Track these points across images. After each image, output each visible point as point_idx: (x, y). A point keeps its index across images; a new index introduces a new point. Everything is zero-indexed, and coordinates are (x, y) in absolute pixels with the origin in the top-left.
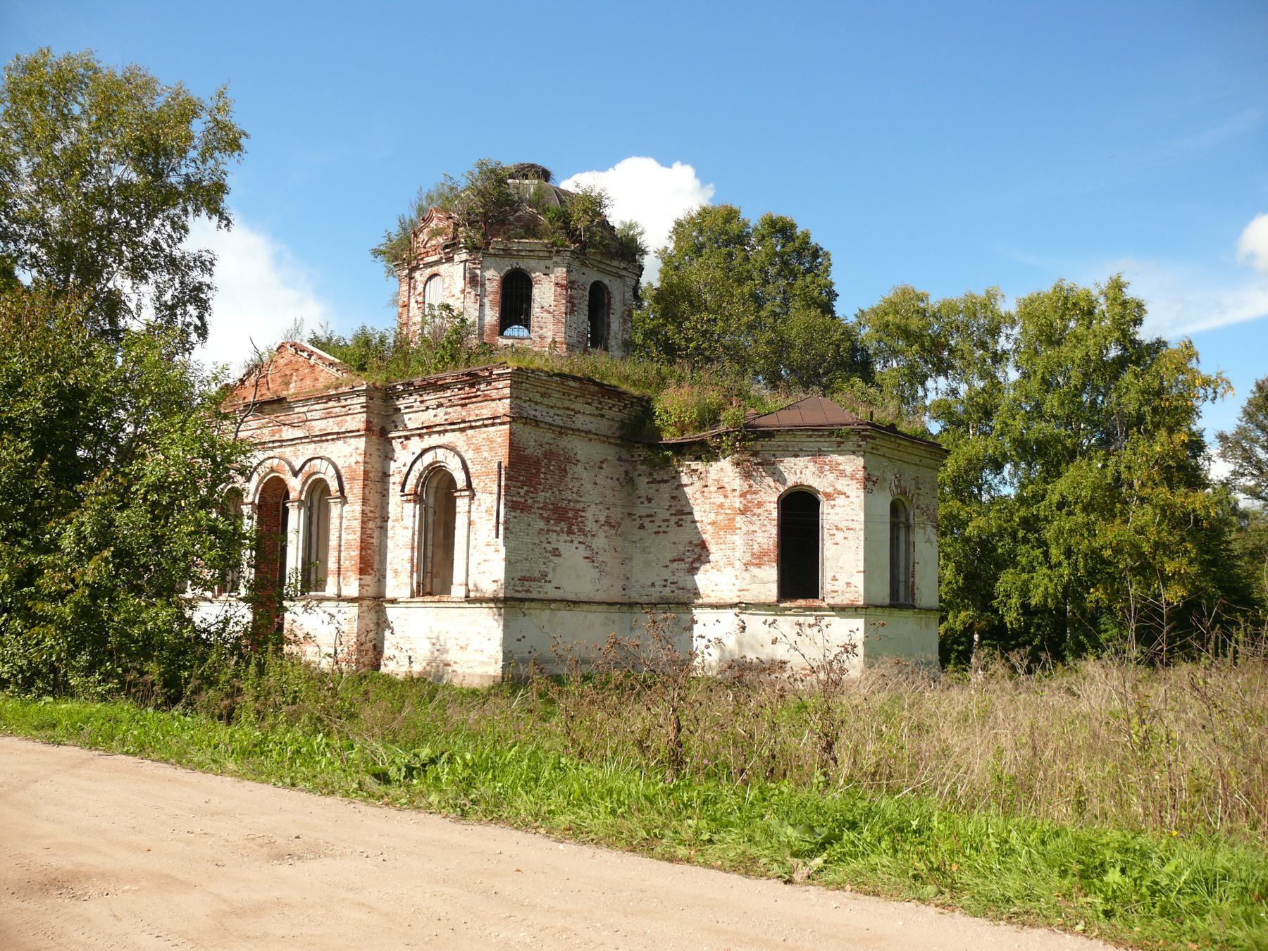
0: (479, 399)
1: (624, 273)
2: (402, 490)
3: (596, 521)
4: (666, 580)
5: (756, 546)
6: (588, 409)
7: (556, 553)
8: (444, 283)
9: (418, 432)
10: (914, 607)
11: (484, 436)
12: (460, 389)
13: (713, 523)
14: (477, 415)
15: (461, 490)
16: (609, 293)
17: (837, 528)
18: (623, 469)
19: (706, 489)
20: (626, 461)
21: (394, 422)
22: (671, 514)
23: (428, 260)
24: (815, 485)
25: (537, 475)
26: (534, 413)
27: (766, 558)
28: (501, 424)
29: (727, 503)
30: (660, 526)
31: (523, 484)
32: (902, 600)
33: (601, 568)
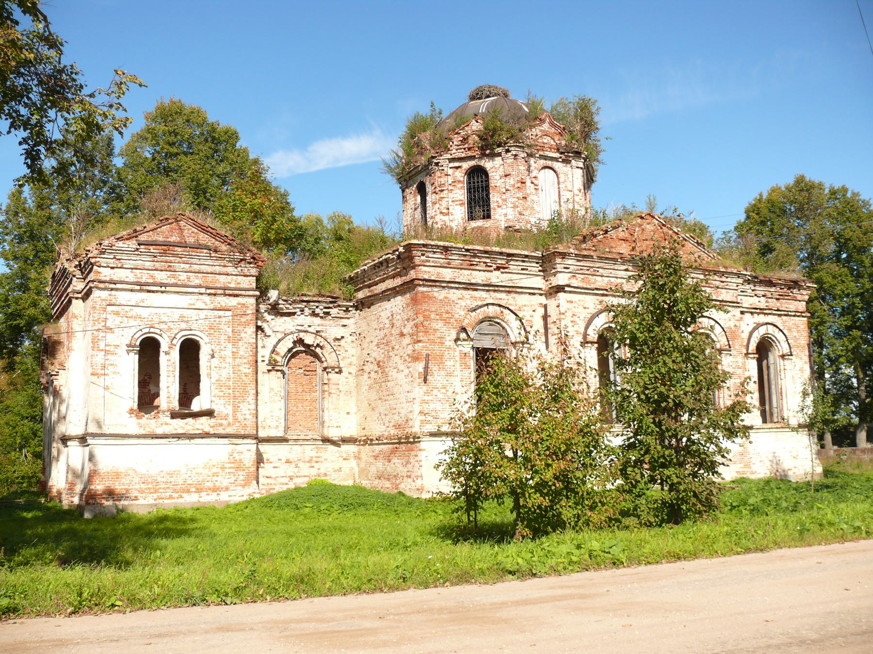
0: (789, 298)
11: (793, 322)
12: (781, 289)
28: (803, 317)
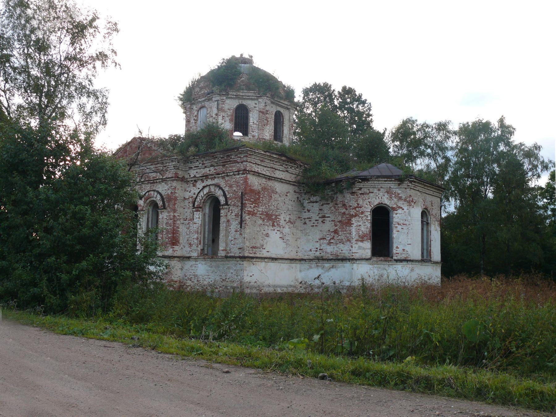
1: (289, 107)
2: (194, 205)
3: (285, 221)
4: (317, 248)
5: (361, 232)
6: (281, 168)
7: (267, 235)
8: (207, 110)
9: (201, 178)
10: (431, 261)
13: (340, 222)
14: (231, 170)
15: (223, 205)
16: (283, 116)
17: (399, 224)
18: (296, 196)
19: (336, 206)
20: (297, 192)
21: (189, 174)
22: (319, 217)
23: (200, 100)
24: (388, 204)
25: (259, 199)
26: (257, 169)
27: (365, 238)
29: (347, 212)
30: (314, 223)
31: (253, 203)
32: (425, 258)
33: (287, 243)
